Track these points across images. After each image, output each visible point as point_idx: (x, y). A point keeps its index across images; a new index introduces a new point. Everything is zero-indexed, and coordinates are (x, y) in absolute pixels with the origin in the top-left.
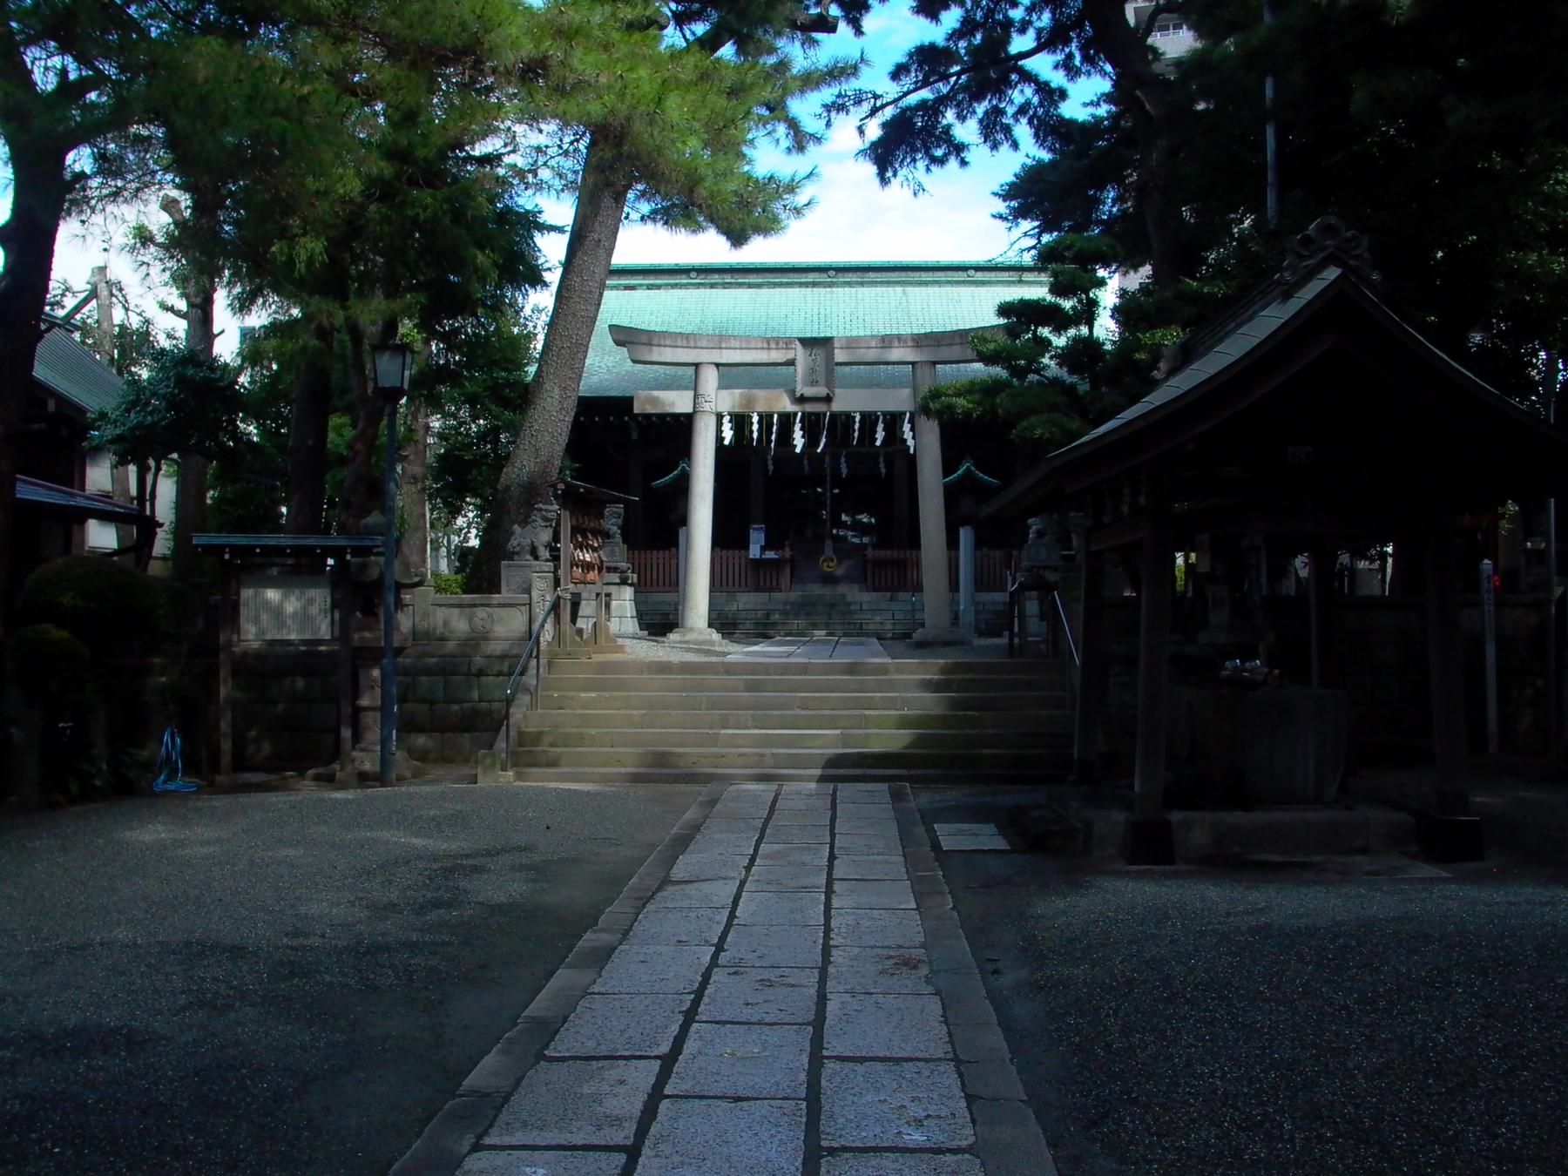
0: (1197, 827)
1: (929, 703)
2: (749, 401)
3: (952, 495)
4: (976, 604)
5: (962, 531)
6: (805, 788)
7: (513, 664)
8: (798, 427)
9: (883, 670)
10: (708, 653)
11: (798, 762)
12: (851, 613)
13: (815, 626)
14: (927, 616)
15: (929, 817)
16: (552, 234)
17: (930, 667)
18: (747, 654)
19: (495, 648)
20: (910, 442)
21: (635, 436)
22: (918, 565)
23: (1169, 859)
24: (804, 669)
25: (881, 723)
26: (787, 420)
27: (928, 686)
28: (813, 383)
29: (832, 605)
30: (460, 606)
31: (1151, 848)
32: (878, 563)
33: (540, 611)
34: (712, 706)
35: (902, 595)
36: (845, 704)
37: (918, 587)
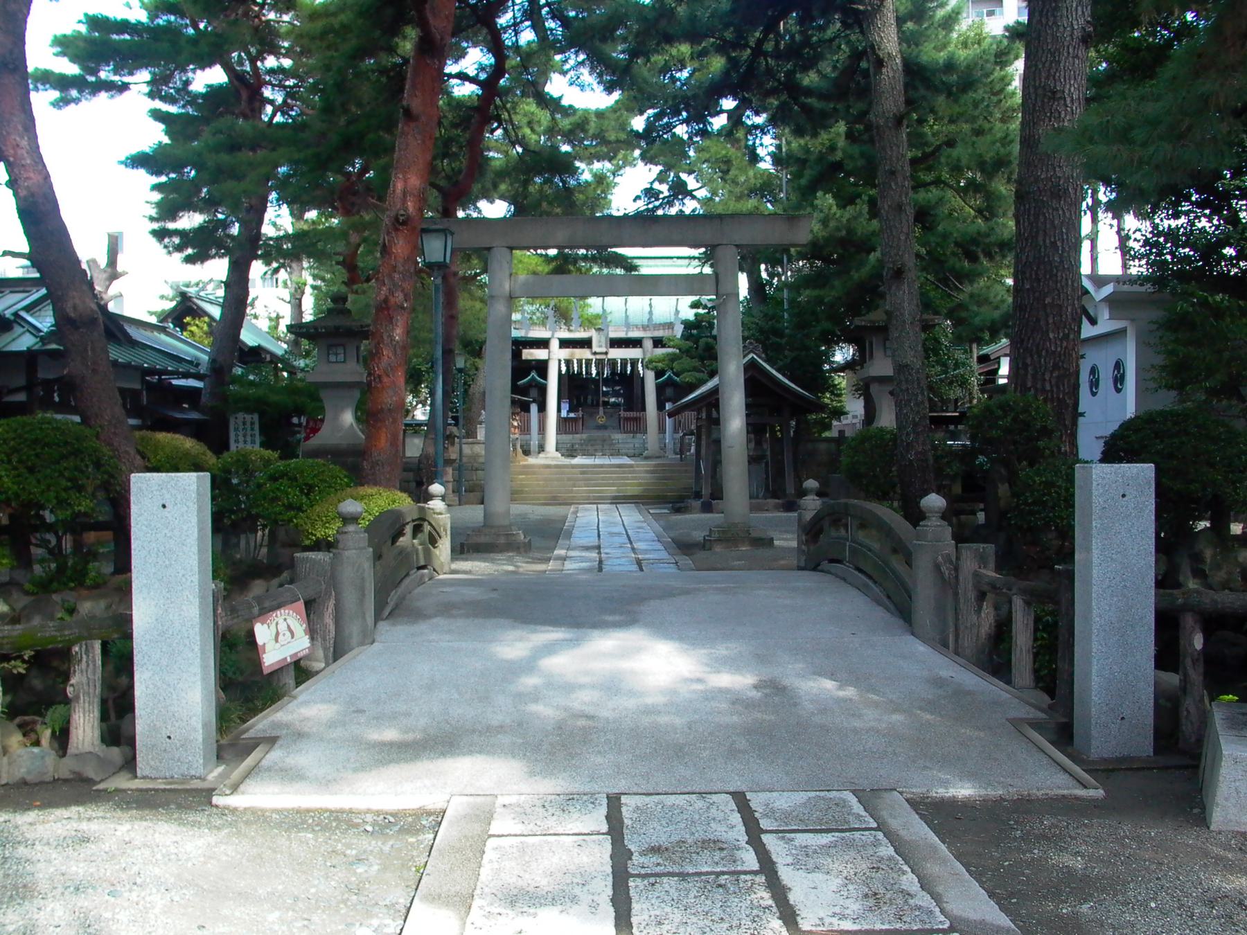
2: (572, 354)
3: (660, 389)
14: (649, 446)
16: (103, 95)
26: (588, 362)
27: (647, 472)
32: (627, 419)
35: (638, 435)
37: (645, 432)
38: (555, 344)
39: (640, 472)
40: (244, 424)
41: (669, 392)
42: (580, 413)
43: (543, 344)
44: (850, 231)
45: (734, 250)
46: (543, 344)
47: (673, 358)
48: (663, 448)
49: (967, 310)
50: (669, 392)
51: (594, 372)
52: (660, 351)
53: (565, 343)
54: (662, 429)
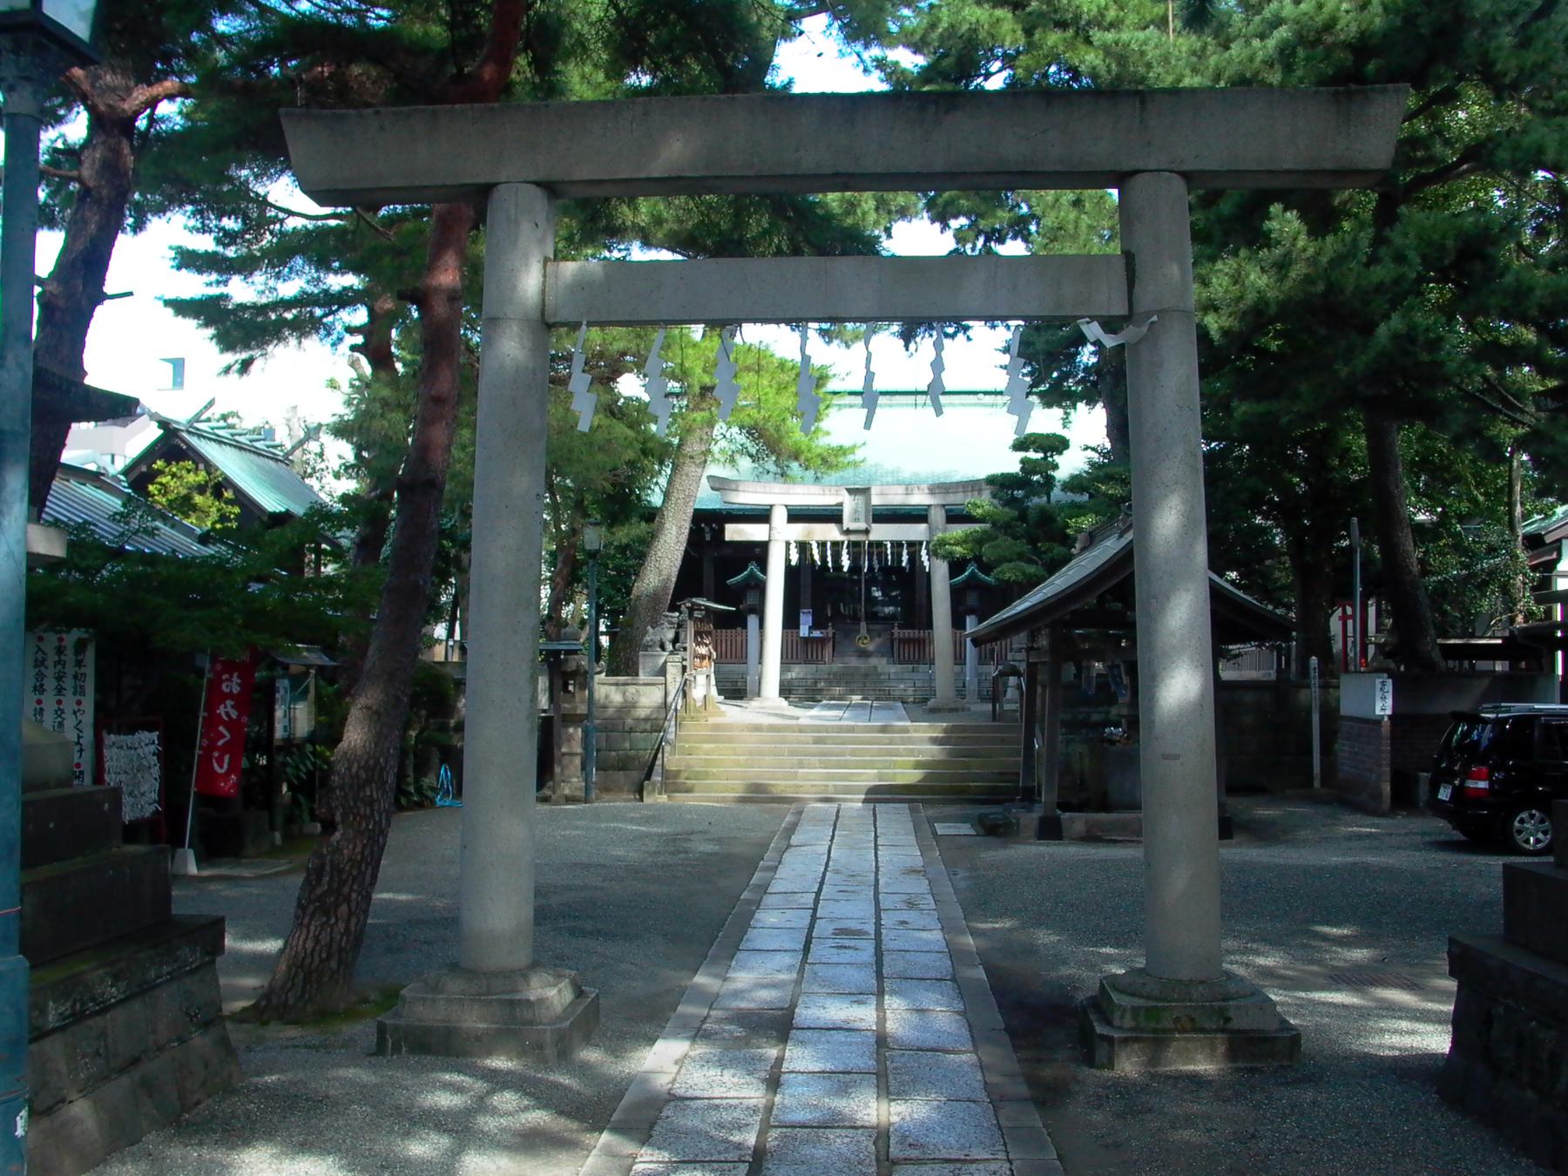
0: (1076, 822)
1: (933, 752)
3: (957, 594)
4: (979, 675)
5: (968, 619)
6: (855, 804)
7: (655, 724)
8: (845, 551)
9: (905, 730)
10: (783, 716)
11: (848, 790)
12: (882, 682)
13: (853, 692)
15: (931, 821)
17: (937, 728)
18: (812, 717)
19: (642, 713)
20: (926, 564)
21: (708, 537)
22: (931, 641)
23: (1061, 838)
24: (852, 729)
25: (903, 765)
26: (836, 545)
27: (934, 741)
28: (856, 520)
29: (866, 675)
30: (617, 684)
31: (1050, 830)
32: (903, 641)
33: (673, 690)
34: (793, 753)
35: (922, 667)
36: (880, 753)
37: (932, 662)
38: (780, 516)
39: (920, 741)
40: (60, 651)
41: (972, 599)
42: (830, 631)
43: (761, 516)
44: (1332, 288)
45: (1179, 185)
46: (761, 516)
47: (980, 540)
48: (961, 692)
49: (1552, 441)
50: (972, 599)
51: (846, 563)
52: (958, 530)
53: (796, 516)
54: (959, 658)
